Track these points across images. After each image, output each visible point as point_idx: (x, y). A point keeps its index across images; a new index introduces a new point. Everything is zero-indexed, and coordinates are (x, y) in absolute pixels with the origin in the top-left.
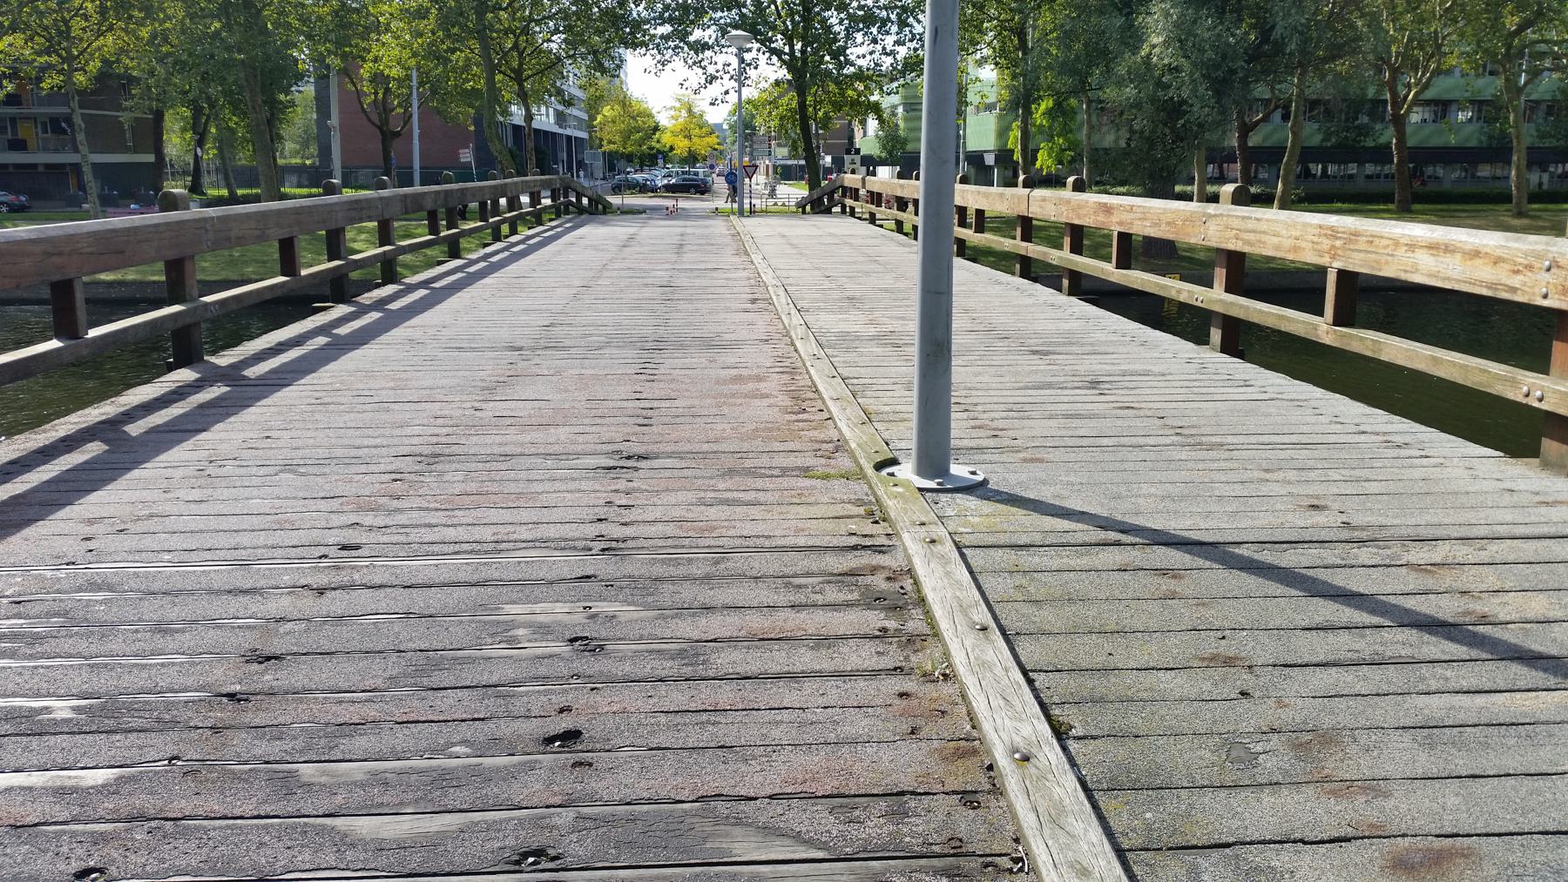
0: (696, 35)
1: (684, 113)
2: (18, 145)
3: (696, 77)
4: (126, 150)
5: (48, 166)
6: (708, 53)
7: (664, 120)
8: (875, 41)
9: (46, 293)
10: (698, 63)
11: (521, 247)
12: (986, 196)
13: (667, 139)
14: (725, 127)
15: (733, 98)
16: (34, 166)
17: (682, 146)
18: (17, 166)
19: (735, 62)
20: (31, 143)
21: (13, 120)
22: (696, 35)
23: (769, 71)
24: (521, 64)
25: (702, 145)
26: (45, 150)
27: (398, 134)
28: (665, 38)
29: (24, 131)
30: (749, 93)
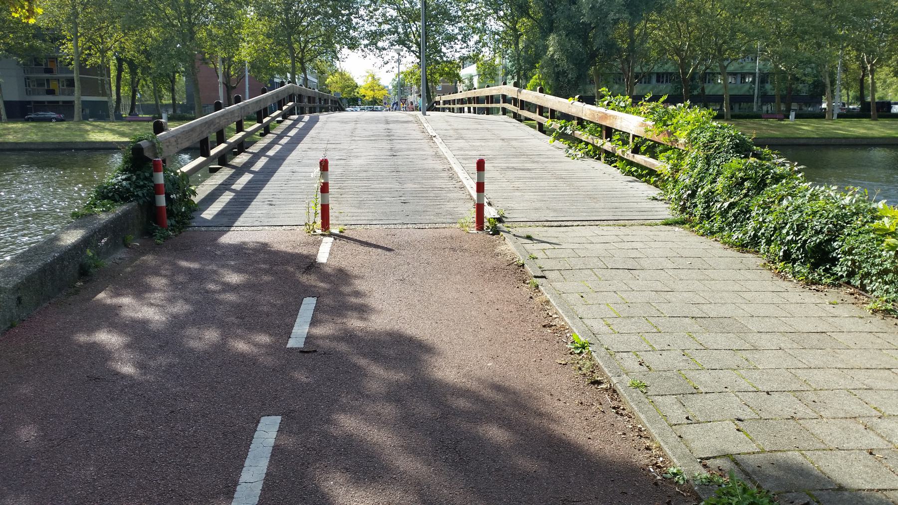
0: (380, 44)
1: (370, 79)
2: (51, 92)
3: (380, 62)
4: (99, 95)
5: (64, 102)
6: (384, 52)
7: (360, 82)
8: (452, 47)
9: (199, 145)
10: (381, 56)
11: (277, 148)
12: (204, 191)
13: (362, 92)
14: (390, 87)
15: (396, 71)
16: (58, 102)
17: (370, 95)
18: (49, 102)
19: (396, 56)
20: (57, 91)
21: (48, 80)
22: (380, 44)
23: (410, 60)
24: (303, 56)
25: (379, 95)
26: (63, 94)
27: (235, 88)
28: (366, 46)
29: (53, 85)
30: (403, 68)
